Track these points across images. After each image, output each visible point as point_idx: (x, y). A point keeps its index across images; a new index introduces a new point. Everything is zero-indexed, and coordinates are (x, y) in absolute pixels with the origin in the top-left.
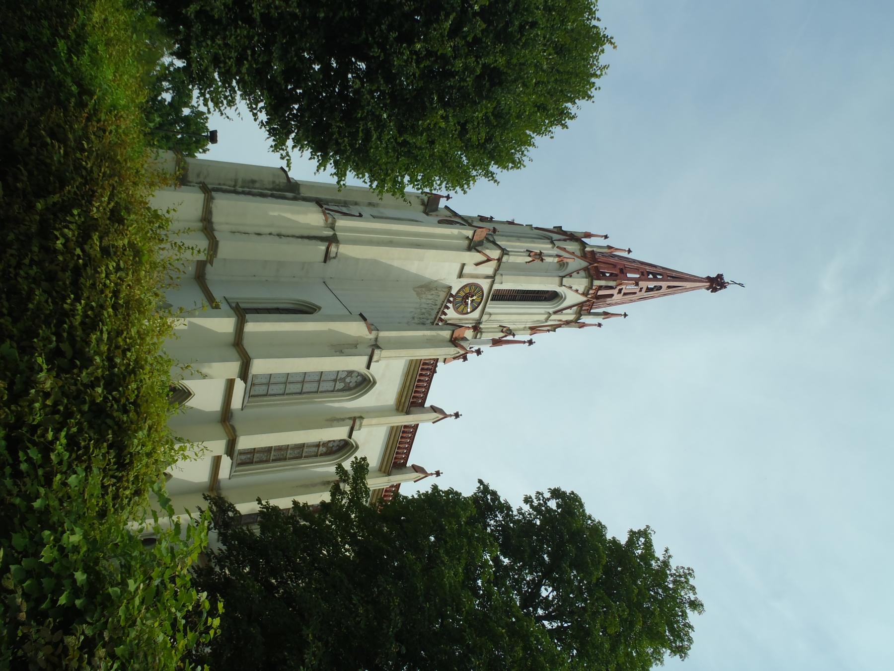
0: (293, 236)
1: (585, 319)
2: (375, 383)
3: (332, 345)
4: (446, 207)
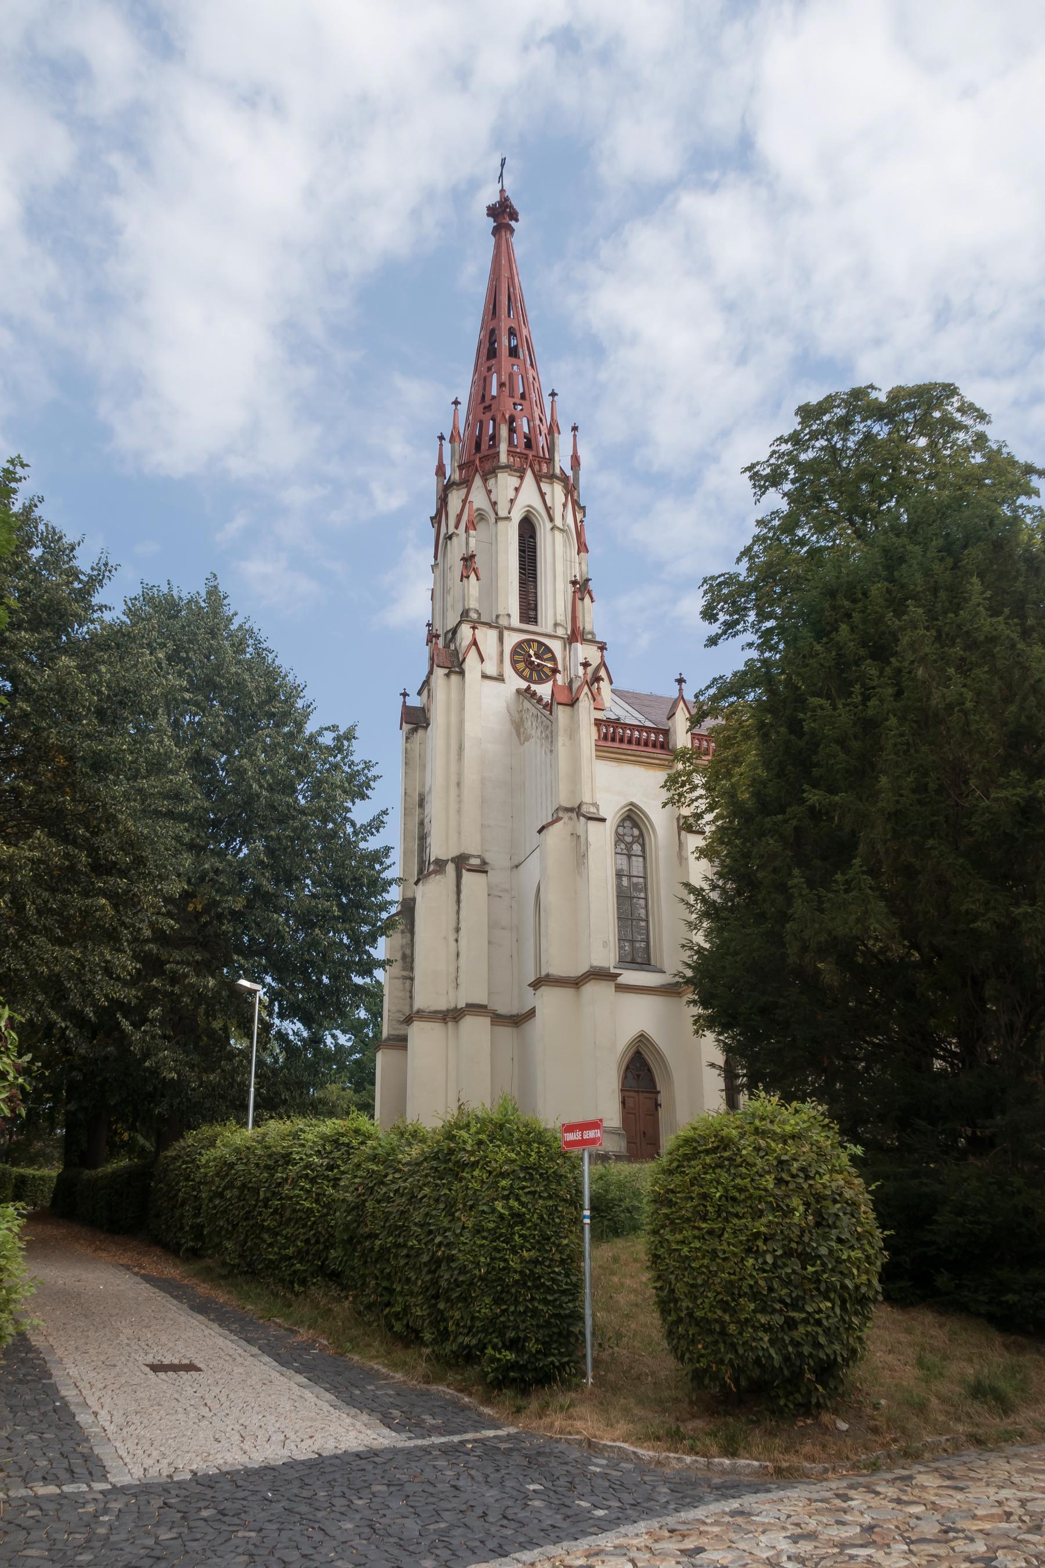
0: (458, 912)
1: (562, 461)
2: (632, 804)
3: (578, 864)
4: (419, 693)
